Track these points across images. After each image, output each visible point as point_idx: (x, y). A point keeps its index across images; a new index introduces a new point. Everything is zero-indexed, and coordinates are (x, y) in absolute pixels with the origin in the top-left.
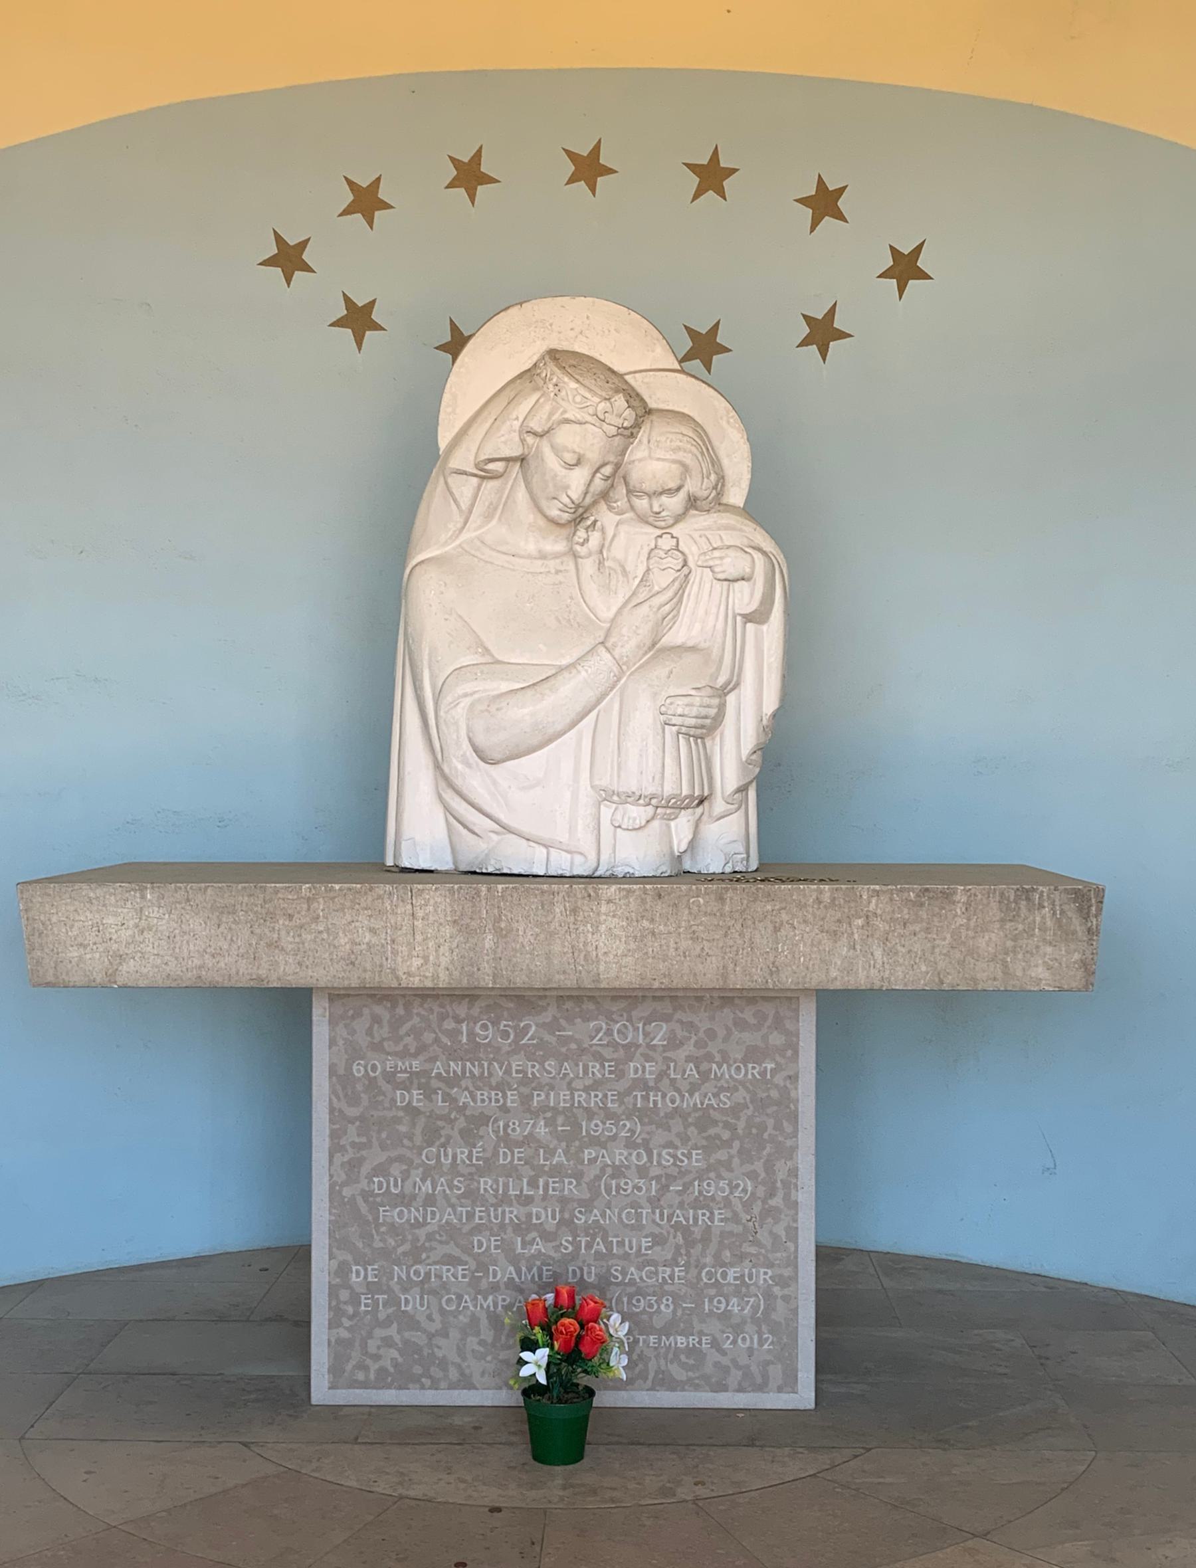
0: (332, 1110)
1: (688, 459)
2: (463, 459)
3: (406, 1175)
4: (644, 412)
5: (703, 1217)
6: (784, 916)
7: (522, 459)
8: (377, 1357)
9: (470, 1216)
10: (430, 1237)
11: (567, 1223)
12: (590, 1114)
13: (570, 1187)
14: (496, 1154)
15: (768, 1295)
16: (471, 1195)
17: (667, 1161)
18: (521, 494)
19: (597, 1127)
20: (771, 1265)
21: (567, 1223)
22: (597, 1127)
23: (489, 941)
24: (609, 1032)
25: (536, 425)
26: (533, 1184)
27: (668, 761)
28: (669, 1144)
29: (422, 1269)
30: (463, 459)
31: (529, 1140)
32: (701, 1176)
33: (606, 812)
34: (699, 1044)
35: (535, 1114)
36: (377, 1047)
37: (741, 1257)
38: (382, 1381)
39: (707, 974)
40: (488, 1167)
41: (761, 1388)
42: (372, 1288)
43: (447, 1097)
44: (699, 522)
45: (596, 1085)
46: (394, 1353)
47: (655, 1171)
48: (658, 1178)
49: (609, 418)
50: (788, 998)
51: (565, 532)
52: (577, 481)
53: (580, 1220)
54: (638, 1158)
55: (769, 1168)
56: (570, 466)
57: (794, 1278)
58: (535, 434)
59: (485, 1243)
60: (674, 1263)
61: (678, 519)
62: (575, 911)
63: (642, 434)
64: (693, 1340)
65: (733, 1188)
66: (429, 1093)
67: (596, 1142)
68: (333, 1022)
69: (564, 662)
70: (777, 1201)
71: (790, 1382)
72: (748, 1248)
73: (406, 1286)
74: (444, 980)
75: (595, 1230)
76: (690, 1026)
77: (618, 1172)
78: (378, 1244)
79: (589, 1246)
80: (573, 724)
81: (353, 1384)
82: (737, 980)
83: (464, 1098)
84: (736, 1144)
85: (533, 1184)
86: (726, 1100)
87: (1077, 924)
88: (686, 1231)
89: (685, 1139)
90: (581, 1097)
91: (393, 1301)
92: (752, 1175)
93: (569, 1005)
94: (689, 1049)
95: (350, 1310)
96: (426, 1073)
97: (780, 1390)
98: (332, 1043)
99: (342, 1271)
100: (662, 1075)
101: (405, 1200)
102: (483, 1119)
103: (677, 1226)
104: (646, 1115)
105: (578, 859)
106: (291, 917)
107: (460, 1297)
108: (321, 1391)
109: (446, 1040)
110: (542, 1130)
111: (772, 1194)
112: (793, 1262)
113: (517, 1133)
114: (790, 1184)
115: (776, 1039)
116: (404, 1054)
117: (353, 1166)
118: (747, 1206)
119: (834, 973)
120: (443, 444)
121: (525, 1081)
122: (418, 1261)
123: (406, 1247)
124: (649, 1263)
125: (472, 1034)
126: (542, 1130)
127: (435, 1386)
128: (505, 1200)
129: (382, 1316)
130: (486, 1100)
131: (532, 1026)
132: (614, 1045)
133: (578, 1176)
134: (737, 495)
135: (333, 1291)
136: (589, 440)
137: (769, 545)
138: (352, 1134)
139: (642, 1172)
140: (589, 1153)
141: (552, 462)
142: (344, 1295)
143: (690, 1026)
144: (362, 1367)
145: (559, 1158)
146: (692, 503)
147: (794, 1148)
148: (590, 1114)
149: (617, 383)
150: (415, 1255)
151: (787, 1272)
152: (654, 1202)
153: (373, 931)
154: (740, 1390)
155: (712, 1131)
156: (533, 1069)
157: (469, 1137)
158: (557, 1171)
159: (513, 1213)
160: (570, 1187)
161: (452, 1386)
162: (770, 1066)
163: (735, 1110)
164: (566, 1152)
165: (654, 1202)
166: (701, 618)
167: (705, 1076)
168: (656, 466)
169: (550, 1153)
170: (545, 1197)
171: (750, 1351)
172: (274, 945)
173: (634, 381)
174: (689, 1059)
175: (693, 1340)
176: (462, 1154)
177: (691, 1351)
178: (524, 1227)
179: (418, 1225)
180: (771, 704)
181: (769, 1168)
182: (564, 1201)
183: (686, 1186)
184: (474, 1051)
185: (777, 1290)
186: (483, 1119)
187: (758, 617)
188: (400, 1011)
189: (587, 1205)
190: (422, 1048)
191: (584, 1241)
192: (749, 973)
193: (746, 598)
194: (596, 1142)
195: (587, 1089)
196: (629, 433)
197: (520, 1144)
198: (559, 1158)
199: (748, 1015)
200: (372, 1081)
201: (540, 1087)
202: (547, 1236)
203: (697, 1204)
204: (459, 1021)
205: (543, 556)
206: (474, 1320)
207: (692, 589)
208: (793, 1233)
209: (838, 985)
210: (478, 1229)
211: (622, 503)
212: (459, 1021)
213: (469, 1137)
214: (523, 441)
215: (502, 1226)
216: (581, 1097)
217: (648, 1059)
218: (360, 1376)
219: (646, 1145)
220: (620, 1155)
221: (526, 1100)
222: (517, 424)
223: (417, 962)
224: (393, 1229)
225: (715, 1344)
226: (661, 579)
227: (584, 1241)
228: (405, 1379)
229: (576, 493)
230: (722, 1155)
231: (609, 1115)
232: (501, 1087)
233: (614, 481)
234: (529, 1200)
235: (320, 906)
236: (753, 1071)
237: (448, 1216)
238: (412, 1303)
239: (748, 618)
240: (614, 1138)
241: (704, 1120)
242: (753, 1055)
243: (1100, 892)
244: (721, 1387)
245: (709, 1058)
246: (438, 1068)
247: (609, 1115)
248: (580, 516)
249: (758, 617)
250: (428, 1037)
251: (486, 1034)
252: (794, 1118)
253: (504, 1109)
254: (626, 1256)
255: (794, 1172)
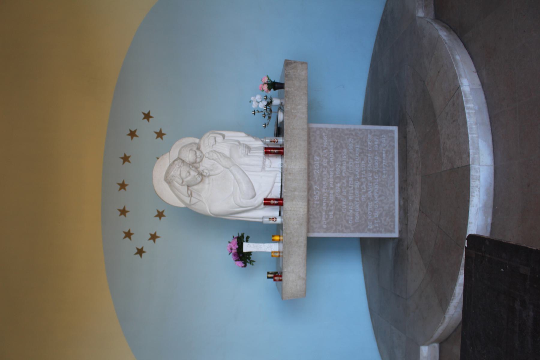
0: (334, 232)
1: (189, 149)
2: (187, 200)
3: (348, 216)
4: (179, 158)
5: (357, 149)
6: (291, 127)
7: (188, 186)
8: (388, 223)
9: (357, 201)
10: (362, 210)
11: (359, 180)
12: (335, 174)
13: (351, 179)
14: (344, 196)
15: (374, 135)
16: (353, 201)
17: (345, 157)
18: (196, 187)
19: (338, 172)
20: (367, 135)
21: (359, 180)
22: (338, 172)
23: (296, 193)
24: (317, 169)
25: (180, 182)
26: (350, 187)
27: (256, 154)
28: (342, 156)
29: (369, 212)
30: (187, 200)
31: (341, 188)
32: (348, 150)
33: (267, 169)
34: (319, 149)
35: (335, 186)
36: (320, 222)
37: (366, 141)
38: (394, 222)
39: (304, 144)
40: (347, 197)
41: (393, 138)
42: (373, 223)
43: (331, 206)
44: (202, 148)
45: (328, 172)
46: (387, 219)
47: (347, 160)
48: (349, 159)
49: (180, 164)
50: (309, 130)
51: (204, 178)
52: (193, 173)
53: (358, 177)
54: (344, 164)
55: (346, 135)
56: (190, 174)
57: (370, 130)
58: (183, 182)
59: (363, 198)
60: (367, 156)
61: (202, 152)
62: (290, 174)
63: (183, 159)
64: (384, 152)
65: (351, 143)
66: (330, 210)
67: (341, 173)
68: (314, 232)
69: (233, 178)
70: (354, 133)
71: (392, 131)
72: (364, 140)
73: (373, 216)
74: (306, 204)
75: (360, 173)
76: (315, 151)
77: (348, 168)
78: (364, 222)
79: (364, 175)
80: (247, 176)
81: (394, 228)
82: (306, 138)
83: (331, 202)
84: (341, 142)
85: (350, 187)
86: (332, 144)
87: (293, 65)
88: (360, 154)
89: (340, 153)
90: (331, 176)
91: (376, 219)
92: (348, 138)
93: (310, 178)
94: (320, 152)
95: (378, 229)
96: (326, 211)
97: (394, 134)
98: (319, 232)
99: (369, 230)
100: (326, 158)
101: (354, 216)
102: (336, 198)
103: (359, 155)
104: (335, 162)
105: (278, 175)
106: (291, 238)
107: (375, 204)
108: (396, 235)
109: (318, 206)
110: (338, 185)
111: (352, 134)
112: (367, 130)
113: (339, 191)
114: (350, 130)
115: (318, 132)
116: (321, 216)
117: (346, 228)
118: (355, 140)
119: (304, 116)
120: (182, 205)
121: (328, 188)
122: (367, 213)
123: (364, 216)
124: (367, 161)
125: (317, 201)
126: (338, 185)
127: (394, 210)
128: (354, 193)
129: (379, 221)
130: (332, 197)
131: (315, 187)
132: (320, 168)
133: (348, 177)
134: (197, 141)
135: (374, 232)
136: (184, 170)
137: (208, 134)
138: (339, 228)
139: (347, 163)
140: (344, 175)
141: (189, 178)
142: (375, 230)
143: (315, 151)
144: (390, 226)
145: (345, 181)
146: (198, 149)
147: (342, 129)
148: (335, 174)
149: (172, 165)
150: (366, 214)
151: (369, 131)
152: (354, 160)
153: (294, 219)
154: (394, 142)
155: (338, 147)
156: (325, 187)
157: (340, 202)
158: (347, 182)
159: (357, 192)
160: (351, 179)
161: (394, 205)
162: (324, 134)
163: (334, 142)
164: (343, 179)
165: (354, 160)
166: (224, 148)
167: (326, 148)
168: (190, 156)
169: (343, 183)
170: (353, 184)
171: (386, 140)
172: (297, 242)
173: (172, 161)
174: (322, 152)
175: (384, 152)
176: (344, 203)
177: (386, 152)
178: (360, 190)
179: (359, 213)
180: (243, 134)
181: (346, 135)
182: (354, 180)
183: (350, 153)
184: (321, 200)
185: (373, 134)
186: (336, 198)
187: (224, 137)
188: (312, 217)
189: (355, 175)
190: (320, 212)
191: (363, 176)
192: (304, 135)
193: (219, 138)
194: (341, 173)
195: (329, 175)
196: (183, 161)
197: (342, 190)
198: (345, 181)
199: (312, 138)
200: (328, 223)
201: (329, 185)
202: (362, 184)
203: (355, 151)
204: (314, 203)
205: (209, 183)
206: (380, 201)
207: (217, 150)
208: (360, 130)
209: (306, 116)
210: (360, 200)
211: (198, 165)
212: (314, 203)
213: (340, 202)
214: (184, 185)
215: (360, 194)
216: (331, 176)
217: (322, 161)
218: (392, 226)
219: (341, 162)
220: (344, 168)
221: (332, 188)
222: (181, 186)
223: (301, 209)
224: (360, 218)
225: (385, 147)
226: (215, 156)
227: (363, 176)
228: (393, 217)
229: (196, 174)
230: (344, 145)
231: (335, 170)
232: (329, 194)
233: (193, 165)
234: (354, 189)
235: (288, 232)
236: (325, 138)
237: (357, 206)
238: (377, 214)
239: (224, 138)
240: (340, 169)
241: (336, 149)
242: (321, 137)
243: (286, 61)
244: (394, 147)
245: (322, 147)
246: (325, 208)
247: (335, 170)
248: (201, 174)
249: (224, 137)
250: (318, 211)
251: (317, 197)
252: (335, 129)
253: (334, 193)
254: (366, 167)
255: (347, 129)
